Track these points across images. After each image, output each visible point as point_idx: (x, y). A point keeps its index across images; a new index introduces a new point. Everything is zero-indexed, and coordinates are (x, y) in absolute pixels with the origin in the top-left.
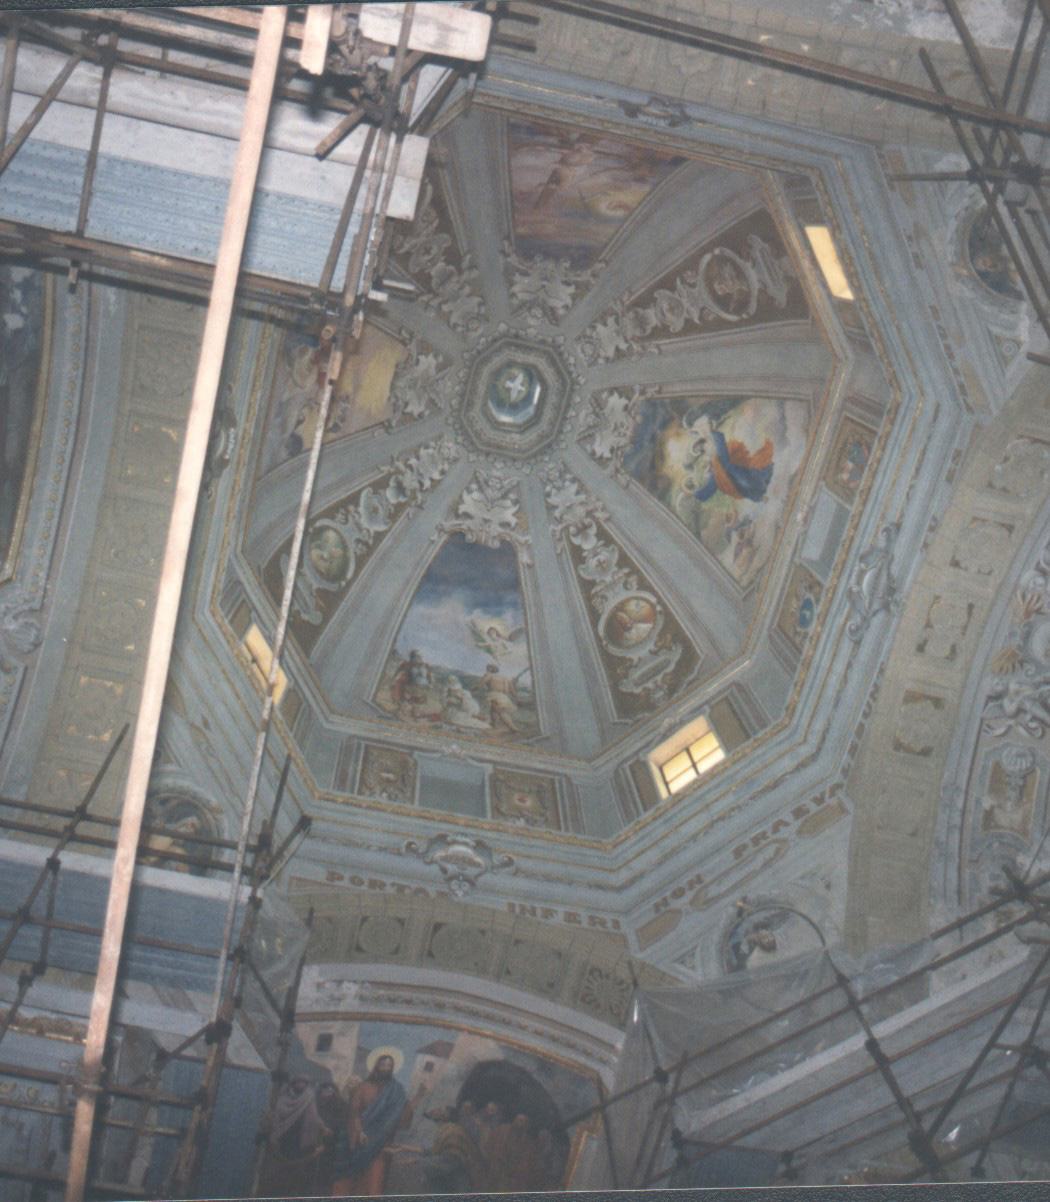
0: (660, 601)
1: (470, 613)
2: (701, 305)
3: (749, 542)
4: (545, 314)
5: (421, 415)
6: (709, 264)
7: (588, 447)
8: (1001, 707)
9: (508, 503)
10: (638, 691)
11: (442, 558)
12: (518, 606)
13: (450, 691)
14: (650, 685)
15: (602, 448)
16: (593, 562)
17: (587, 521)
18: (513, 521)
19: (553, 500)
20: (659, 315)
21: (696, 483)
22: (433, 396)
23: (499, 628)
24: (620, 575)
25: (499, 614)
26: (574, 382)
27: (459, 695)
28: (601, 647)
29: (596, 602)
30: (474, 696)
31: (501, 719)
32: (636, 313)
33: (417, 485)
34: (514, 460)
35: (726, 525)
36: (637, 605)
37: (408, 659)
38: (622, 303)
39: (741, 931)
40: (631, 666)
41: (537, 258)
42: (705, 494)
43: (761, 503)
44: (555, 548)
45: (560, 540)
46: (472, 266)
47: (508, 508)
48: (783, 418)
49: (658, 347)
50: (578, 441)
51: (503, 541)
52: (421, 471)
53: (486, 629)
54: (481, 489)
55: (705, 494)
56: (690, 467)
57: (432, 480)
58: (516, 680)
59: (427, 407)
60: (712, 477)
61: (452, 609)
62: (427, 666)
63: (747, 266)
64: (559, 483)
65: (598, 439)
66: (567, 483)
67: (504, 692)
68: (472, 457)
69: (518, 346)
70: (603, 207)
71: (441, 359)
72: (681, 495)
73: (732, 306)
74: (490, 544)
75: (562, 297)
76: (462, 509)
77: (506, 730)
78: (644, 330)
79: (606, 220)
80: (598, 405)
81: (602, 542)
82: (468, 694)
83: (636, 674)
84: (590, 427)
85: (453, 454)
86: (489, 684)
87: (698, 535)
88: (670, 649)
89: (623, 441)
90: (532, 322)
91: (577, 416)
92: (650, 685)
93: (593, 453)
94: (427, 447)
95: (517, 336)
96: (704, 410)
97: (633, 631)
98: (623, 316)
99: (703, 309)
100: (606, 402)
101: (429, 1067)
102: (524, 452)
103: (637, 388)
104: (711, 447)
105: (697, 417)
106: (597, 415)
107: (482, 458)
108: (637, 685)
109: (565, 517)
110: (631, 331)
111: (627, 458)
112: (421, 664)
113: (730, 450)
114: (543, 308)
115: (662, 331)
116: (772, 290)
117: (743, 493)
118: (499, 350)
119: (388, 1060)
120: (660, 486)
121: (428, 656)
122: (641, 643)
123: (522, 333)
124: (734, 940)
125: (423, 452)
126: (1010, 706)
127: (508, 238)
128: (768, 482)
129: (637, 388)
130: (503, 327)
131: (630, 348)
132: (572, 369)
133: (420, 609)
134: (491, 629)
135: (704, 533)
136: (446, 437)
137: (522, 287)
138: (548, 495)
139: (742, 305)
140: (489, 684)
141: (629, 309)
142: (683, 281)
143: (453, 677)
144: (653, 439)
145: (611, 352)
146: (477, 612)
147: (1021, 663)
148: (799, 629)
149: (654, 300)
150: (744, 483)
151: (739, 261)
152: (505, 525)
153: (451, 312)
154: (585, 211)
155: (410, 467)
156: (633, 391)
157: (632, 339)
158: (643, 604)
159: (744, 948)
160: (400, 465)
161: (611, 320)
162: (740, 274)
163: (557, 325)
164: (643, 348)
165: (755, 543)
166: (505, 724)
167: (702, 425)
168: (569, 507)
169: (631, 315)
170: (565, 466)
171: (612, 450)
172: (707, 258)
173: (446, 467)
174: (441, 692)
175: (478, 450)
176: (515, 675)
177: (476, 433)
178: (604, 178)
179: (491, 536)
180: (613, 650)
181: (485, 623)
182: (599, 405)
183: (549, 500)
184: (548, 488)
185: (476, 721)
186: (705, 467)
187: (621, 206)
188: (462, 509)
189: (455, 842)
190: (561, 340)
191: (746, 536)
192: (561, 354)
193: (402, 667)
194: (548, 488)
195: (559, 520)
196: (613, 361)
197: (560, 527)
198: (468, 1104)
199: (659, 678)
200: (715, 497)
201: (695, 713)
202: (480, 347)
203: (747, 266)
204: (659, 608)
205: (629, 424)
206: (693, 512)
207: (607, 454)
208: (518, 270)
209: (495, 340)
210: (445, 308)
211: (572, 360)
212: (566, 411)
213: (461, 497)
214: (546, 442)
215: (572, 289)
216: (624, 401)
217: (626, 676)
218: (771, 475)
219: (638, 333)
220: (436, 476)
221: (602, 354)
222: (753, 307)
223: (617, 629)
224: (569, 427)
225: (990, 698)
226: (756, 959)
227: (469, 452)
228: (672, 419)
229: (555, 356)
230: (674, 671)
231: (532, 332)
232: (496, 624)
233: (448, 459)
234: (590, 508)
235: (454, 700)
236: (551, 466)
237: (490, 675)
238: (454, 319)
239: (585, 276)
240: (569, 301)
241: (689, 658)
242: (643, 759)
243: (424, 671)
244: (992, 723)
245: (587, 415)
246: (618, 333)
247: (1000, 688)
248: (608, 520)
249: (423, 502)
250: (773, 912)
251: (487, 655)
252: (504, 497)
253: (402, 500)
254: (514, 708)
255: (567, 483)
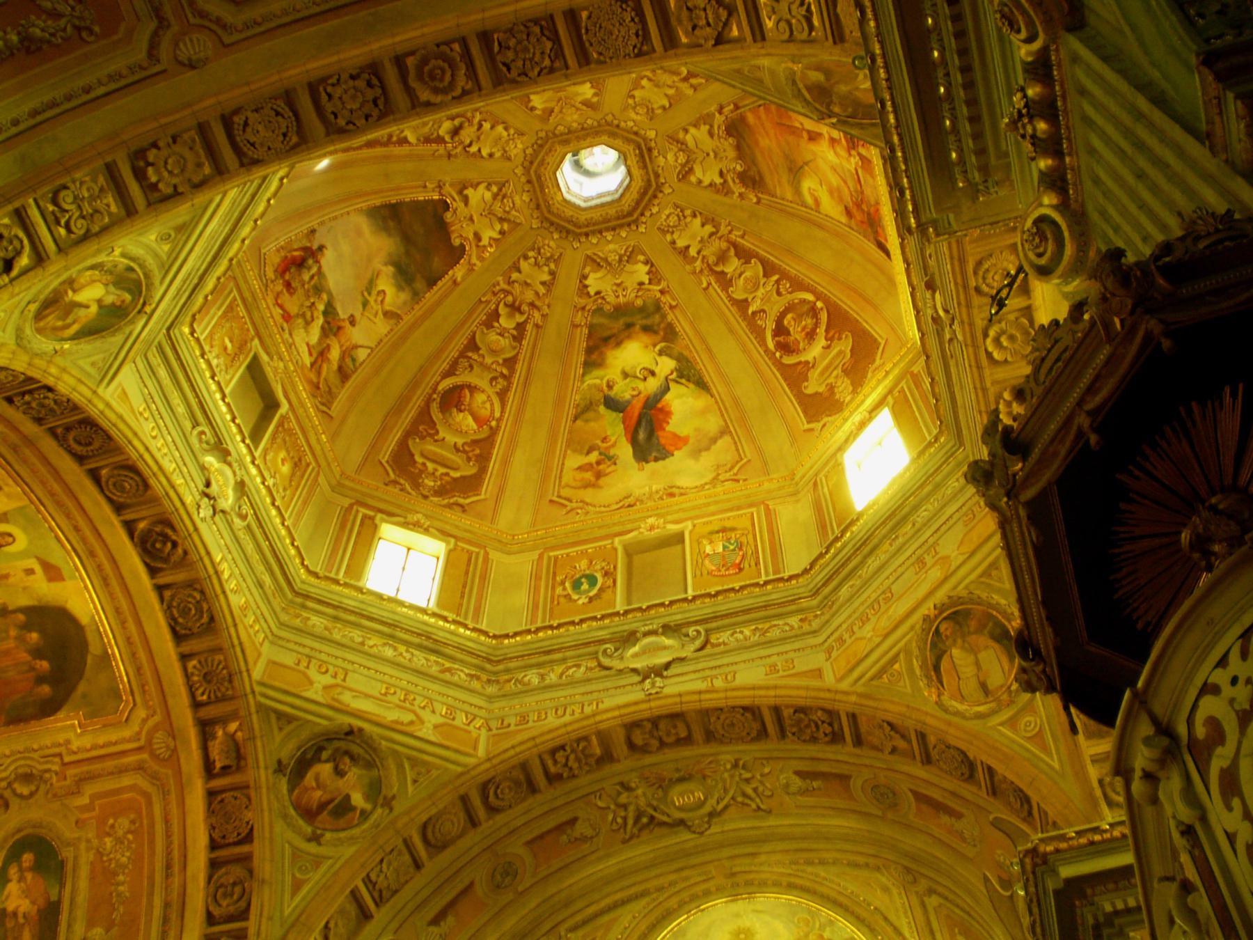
0: (499, 420)
1: (386, 264)
2: (766, 308)
3: (599, 475)
4: (683, 166)
5: (533, 109)
6: (804, 301)
7: (587, 269)
8: (619, 794)
9: (498, 227)
10: (419, 459)
11: (417, 207)
12: (416, 296)
13: (313, 304)
14: (430, 466)
15: (594, 282)
16: (493, 336)
17: (525, 308)
18: (485, 241)
19: (524, 265)
20: (738, 271)
21: (615, 388)
22: (557, 110)
23: (388, 299)
24: (499, 369)
25: (400, 288)
26: (636, 222)
27: (315, 314)
28: (429, 401)
29: (464, 363)
30: (323, 328)
31: (320, 367)
32: (729, 249)
33: (467, 142)
34: (538, 207)
35: (599, 442)
36: (484, 403)
37: (315, 247)
38: (730, 232)
39: (336, 744)
40: (432, 436)
41: (731, 140)
42: (612, 404)
43: (636, 465)
44: (484, 295)
45: (495, 294)
46: (695, 88)
47: (493, 229)
48: (714, 440)
49: (709, 284)
50: (588, 257)
51: (462, 247)
52: (482, 137)
53: (380, 288)
54: (495, 197)
55: (612, 404)
56: (626, 375)
57: (479, 150)
58: (356, 347)
59: (544, 110)
60: (629, 402)
61: (379, 246)
62: (320, 268)
63: (821, 342)
64: (541, 261)
65: (599, 275)
66: (546, 269)
67: (341, 346)
68: (519, 171)
69: (642, 156)
70: (808, 184)
71: (595, 99)
72: (598, 381)
73: (781, 339)
74: (453, 236)
75: (707, 174)
76: (469, 192)
77: (315, 380)
78: (717, 264)
79: (798, 192)
80: (629, 257)
81: (515, 333)
82: (320, 321)
83: (430, 447)
84: (606, 260)
85: (513, 153)
86: (339, 328)
87: (576, 418)
88: (469, 459)
89: (611, 299)
90: (670, 157)
91: (610, 242)
92: (430, 466)
93: (585, 277)
94: (506, 129)
95: (650, 150)
96: (680, 358)
97: (461, 415)
98: (720, 238)
99: (764, 311)
100: (636, 263)
101: (30, 572)
102: (549, 212)
103: (663, 285)
104: (652, 385)
105: (670, 356)
106: (620, 260)
107: (523, 179)
108: (422, 455)
109: (516, 285)
110: (710, 252)
111: (599, 310)
112: (317, 262)
113: (659, 406)
114: (687, 162)
115: (725, 282)
116: (814, 375)
117: (634, 441)
118: (629, 141)
119: (11, 540)
120: (594, 357)
121: (328, 260)
122: (460, 432)
123: (655, 153)
124: (325, 744)
125: (500, 128)
126: (623, 799)
127: (737, 107)
128: (656, 460)
129: (663, 285)
130: (652, 134)
131: (694, 259)
132: (647, 214)
133: (364, 223)
134: (383, 291)
135: (579, 422)
136: (525, 138)
137: (697, 136)
138: (526, 258)
139: (786, 348)
140: (339, 328)
141: (728, 241)
142: (777, 282)
143: (325, 296)
144: (629, 326)
145: (681, 243)
146: (391, 269)
147: (660, 787)
148: (567, 585)
149: (748, 262)
150: (642, 436)
151: (821, 330)
152: (478, 237)
153: (643, 87)
154: (796, 170)
155: (480, 126)
156: (659, 283)
157: (704, 257)
158: (488, 405)
159: (325, 755)
160: (478, 117)
161: (709, 228)
162: (811, 335)
163: (679, 180)
164: (701, 271)
165: (602, 481)
166: (319, 373)
167: (666, 365)
168: (527, 284)
169: (724, 245)
170: (560, 257)
171: (598, 293)
172: (810, 297)
173: (498, 155)
174: (308, 297)
175: (529, 172)
176: (360, 343)
177: (543, 160)
178: (835, 180)
179: (461, 232)
180: (435, 408)
181: (386, 284)
182: (629, 257)
183: (522, 261)
184: (531, 254)
185: (306, 349)
186: (634, 389)
187: (817, 202)
188: (469, 192)
189: (230, 465)
190: (667, 190)
191: (601, 467)
192: (655, 197)
193: (305, 249)
194: (531, 254)
195: (510, 283)
196: (675, 249)
197: (503, 286)
198: (21, 617)
199: (442, 470)
200: (614, 414)
201: (444, 534)
202: (623, 124)
203: (821, 342)
204: (494, 423)
205: (629, 295)
206: (591, 403)
207: (592, 291)
208: (711, 126)
209: (636, 134)
210: (644, 82)
211: (655, 210)
212: (607, 229)
213: (479, 184)
214: (570, 227)
215: (719, 181)
216: (646, 279)
217: (423, 438)
218: (663, 459)
219: (712, 259)
220: (485, 153)
221: (675, 236)
222: (789, 360)
223: (453, 399)
224: (594, 241)
225: (622, 784)
226: (325, 769)
227: (522, 165)
228: (656, 333)
229: (650, 192)
230: (455, 480)
231: (661, 161)
232: (390, 291)
233: (505, 151)
234: (538, 303)
235: (308, 314)
236: (552, 244)
237: (347, 324)
238: (637, 93)
239: (738, 189)
240: (706, 182)
241: (470, 484)
242: (377, 521)
243: (314, 270)
244: (604, 797)
245: (615, 251)
246: (702, 241)
247: (633, 785)
248: (537, 326)
249: (456, 156)
250: (367, 757)
251: (361, 307)
252: (501, 220)
253: (447, 138)
254: (335, 367)
255: (546, 269)
